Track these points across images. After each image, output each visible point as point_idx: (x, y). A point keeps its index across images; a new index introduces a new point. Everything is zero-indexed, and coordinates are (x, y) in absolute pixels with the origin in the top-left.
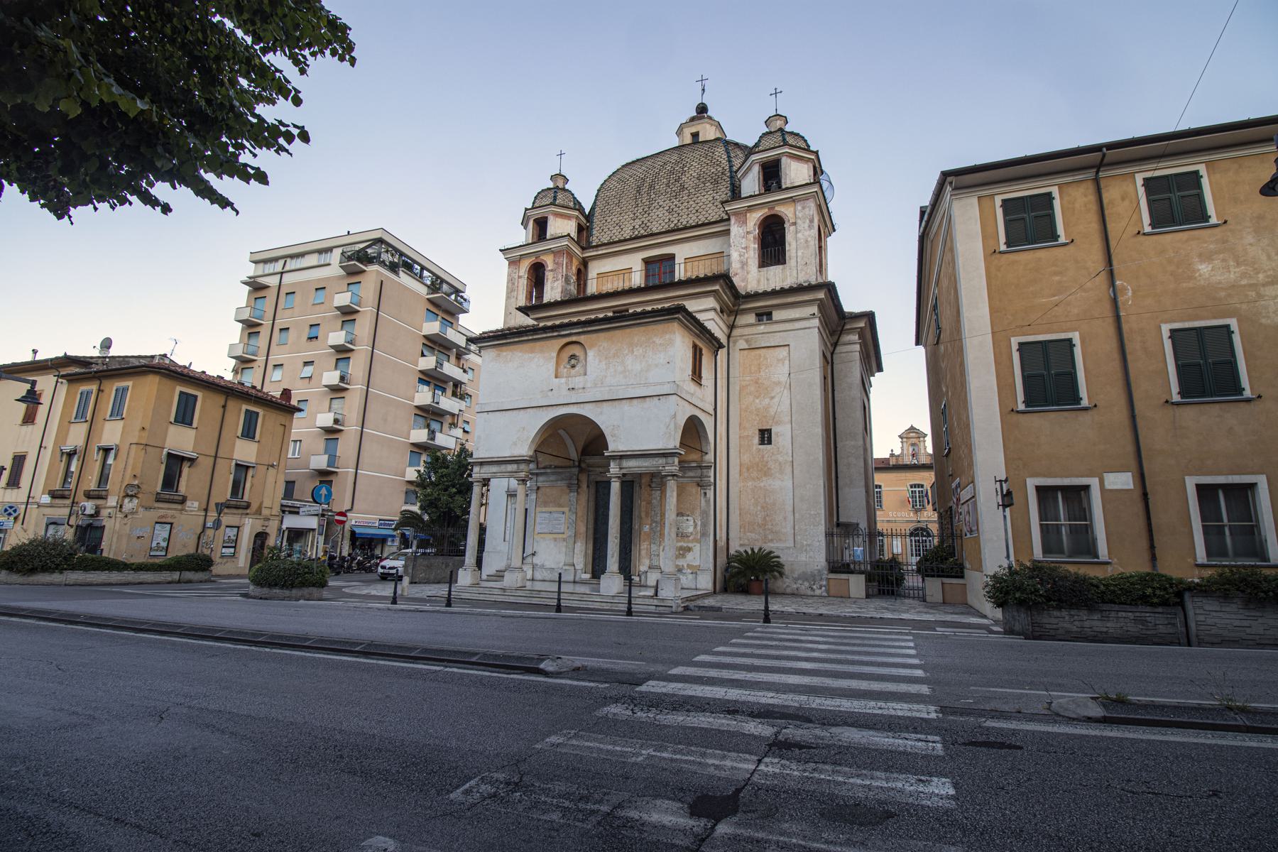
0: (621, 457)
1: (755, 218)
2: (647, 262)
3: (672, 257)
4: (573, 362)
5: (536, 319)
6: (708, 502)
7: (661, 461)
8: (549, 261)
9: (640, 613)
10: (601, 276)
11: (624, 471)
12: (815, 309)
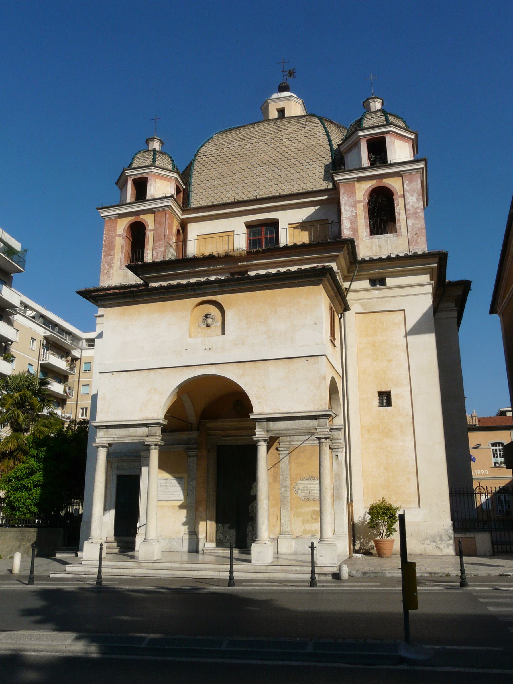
0: (269, 420)
1: (363, 190)
2: (249, 226)
7: (145, 430)
8: (149, 220)
9: (242, 582)
10: (201, 237)
11: (271, 434)
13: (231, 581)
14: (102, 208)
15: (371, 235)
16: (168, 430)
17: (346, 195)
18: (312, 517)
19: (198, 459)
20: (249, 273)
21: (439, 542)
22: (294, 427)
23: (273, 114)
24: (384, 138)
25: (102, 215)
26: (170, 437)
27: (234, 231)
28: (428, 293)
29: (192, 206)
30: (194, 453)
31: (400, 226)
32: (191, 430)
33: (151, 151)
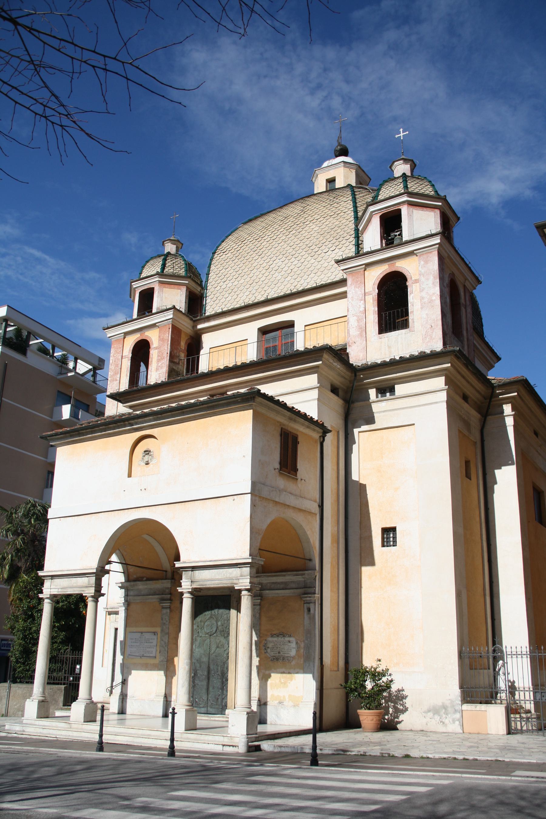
0: (194, 568)
1: (375, 275)
3: (290, 325)
4: (147, 458)
5: (131, 407)
6: (313, 619)
11: (195, 586)
12: (442, 379)
13: (101, 746)
14: (108, 328)
15: (379, 334)
16: (145, 579)
17: (353, 287)
18: (280, 681)
19: (171, 611)
20: (228, 393)
21: (444, 716)
22: (217, 577)
23: (320, 185)
24: (399, 211)
25: (108, 336)
26: (146, 587)
27: (479, 282)
28: (442, 402)
29: (207, 314)
30: (167, 604)
31: (413, 319)
32: (166, 579)
33: (398, 178)
